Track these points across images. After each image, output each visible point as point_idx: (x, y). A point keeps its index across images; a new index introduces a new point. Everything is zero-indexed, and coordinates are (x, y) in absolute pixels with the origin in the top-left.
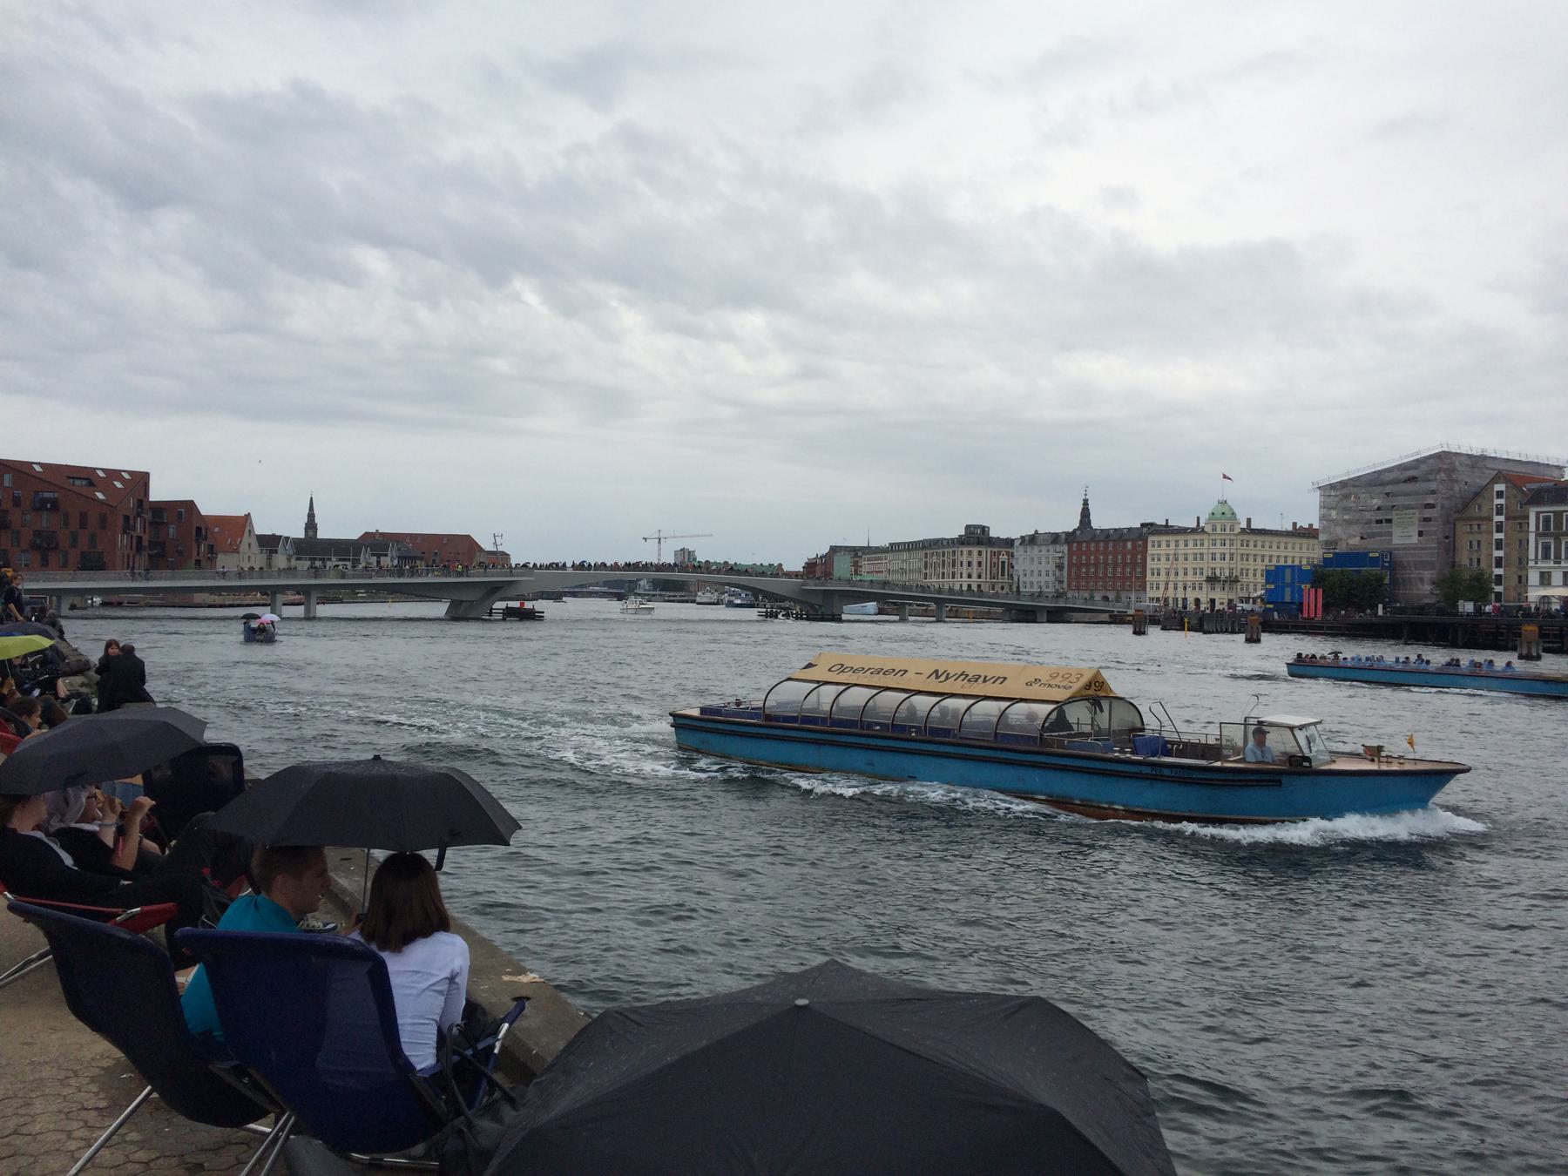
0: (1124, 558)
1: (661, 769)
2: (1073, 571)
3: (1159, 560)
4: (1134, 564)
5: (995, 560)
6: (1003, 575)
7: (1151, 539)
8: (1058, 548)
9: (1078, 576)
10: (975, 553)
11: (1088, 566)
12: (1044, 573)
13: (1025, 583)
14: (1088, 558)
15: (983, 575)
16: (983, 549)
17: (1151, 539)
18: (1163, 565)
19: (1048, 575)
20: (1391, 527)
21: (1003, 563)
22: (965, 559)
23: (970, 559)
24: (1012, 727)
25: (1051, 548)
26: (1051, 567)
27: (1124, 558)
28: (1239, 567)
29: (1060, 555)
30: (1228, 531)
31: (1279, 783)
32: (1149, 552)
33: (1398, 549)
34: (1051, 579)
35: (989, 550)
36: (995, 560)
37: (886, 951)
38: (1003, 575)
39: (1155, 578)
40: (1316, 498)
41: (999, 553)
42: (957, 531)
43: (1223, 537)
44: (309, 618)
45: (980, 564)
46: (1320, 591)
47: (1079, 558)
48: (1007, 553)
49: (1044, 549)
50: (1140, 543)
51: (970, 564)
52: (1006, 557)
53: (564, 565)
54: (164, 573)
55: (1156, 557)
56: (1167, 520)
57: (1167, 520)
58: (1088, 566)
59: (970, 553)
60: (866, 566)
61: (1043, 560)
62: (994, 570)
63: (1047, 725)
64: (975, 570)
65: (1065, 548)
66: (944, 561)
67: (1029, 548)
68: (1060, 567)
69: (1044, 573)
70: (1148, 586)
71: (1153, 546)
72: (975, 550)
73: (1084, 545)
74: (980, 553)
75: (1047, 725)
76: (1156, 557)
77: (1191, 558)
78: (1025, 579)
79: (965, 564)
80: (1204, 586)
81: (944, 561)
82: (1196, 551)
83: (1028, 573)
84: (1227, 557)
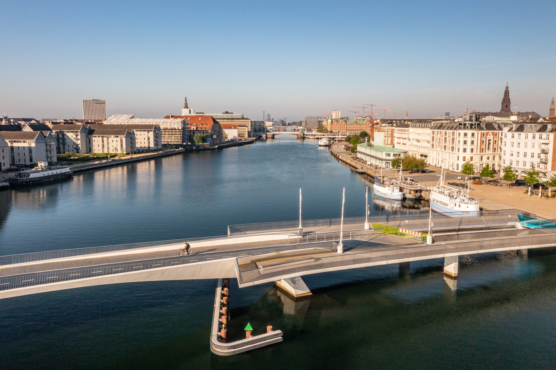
1: (345, 151)
16: (475, 132)
22: (462, 139)
24: (126, 165)
25: (537, 135)
31: (226, 112)
35: (480, 132)
37: (494, 202)
41: (487, 134)
42: (525, 112)
45: (472, 142)
48: (493, 134)
49: (530, 135)
51: (465, 142)
52: (492, 136)
59: (466, 135)
60: (97, 141)
63: (279, 293)
64: (469, 147)
66: (445, 138)
67: (516, 134)
72: (469, 132)
74: (473, 135)
75: (279, 293)
81: (445, 138)
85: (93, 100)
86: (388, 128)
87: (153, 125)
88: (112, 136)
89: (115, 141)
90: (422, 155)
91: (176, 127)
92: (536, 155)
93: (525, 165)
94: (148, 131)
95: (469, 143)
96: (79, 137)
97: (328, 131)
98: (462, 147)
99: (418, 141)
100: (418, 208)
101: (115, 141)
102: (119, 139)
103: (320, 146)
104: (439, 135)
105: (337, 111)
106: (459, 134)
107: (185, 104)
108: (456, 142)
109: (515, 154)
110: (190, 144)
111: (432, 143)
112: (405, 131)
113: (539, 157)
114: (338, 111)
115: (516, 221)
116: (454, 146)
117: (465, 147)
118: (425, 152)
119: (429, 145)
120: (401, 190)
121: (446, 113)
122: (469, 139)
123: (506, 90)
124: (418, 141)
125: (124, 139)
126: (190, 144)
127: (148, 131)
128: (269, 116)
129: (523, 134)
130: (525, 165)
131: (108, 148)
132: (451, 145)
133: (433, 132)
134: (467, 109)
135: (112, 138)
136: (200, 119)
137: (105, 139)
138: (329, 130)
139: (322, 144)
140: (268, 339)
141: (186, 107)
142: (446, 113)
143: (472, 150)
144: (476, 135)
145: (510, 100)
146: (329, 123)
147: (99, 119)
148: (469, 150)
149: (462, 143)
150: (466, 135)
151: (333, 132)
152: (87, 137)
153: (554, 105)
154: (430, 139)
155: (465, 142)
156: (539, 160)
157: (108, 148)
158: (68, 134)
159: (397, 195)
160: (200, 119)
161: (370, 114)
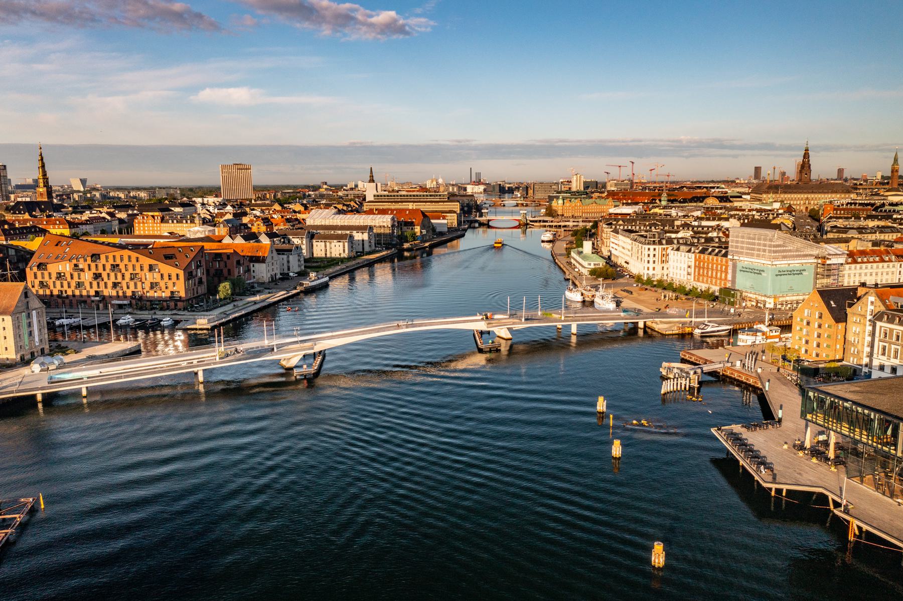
22: (647, 253)
35: (661, 247)
41: (667, 248)
45: (654, 255)
51: (649, 255)
59: (649, 249)
64: (651, 259)
67: (676, 252)
74: (655, 249)
85: (235, 164)
86: (607, 230)
87: (367, 226)
88: (335, 241)
89: (337, 246)
90: (626, 262)
91: (385, 224)
93: (680, 276)
94: (363, 233)
95: (652, 256)
96: (304, 242)
97: (558, 215)
98: (646, 259)
99: (623, 248)
101: (337, 246)
102: (341, 244)
103: (543, 241)
105: (578, 175)
107: (370, 176)
112: (616, 237)
115: (620, 312)
117: (649, 259)
118: (628, 259)
119: (629, 253)
120: (582, 294)
121: (756, 167)
122: (652, 253)
123: (805, 154)
124: (623, 248)
125: (346, 244)
127: (363, 233)
128: (478, 175)
130: (680, 276)
131: (331, 253)
134: (774, 169)
135: (335, 242)
136: (407, 212)
137: (328, 244)
138: (560, 213)
139: (546, 239)
141: (372, 180)
142: (756, 167)
143: (654, 262)
144: (657, 250)
145: (811, 167)
146: (560, 205)
148: (651, 262)
149: (646, 255)
150: (649, 249)
151: (565, 215)
152: (310, 242)
153: (898, 165)
154: (630, 249)
155: (649, 255)
157: (331, 253)
158: (293, 240)
159: (580, 298)
160: (407, 212)
161: (631, 177)
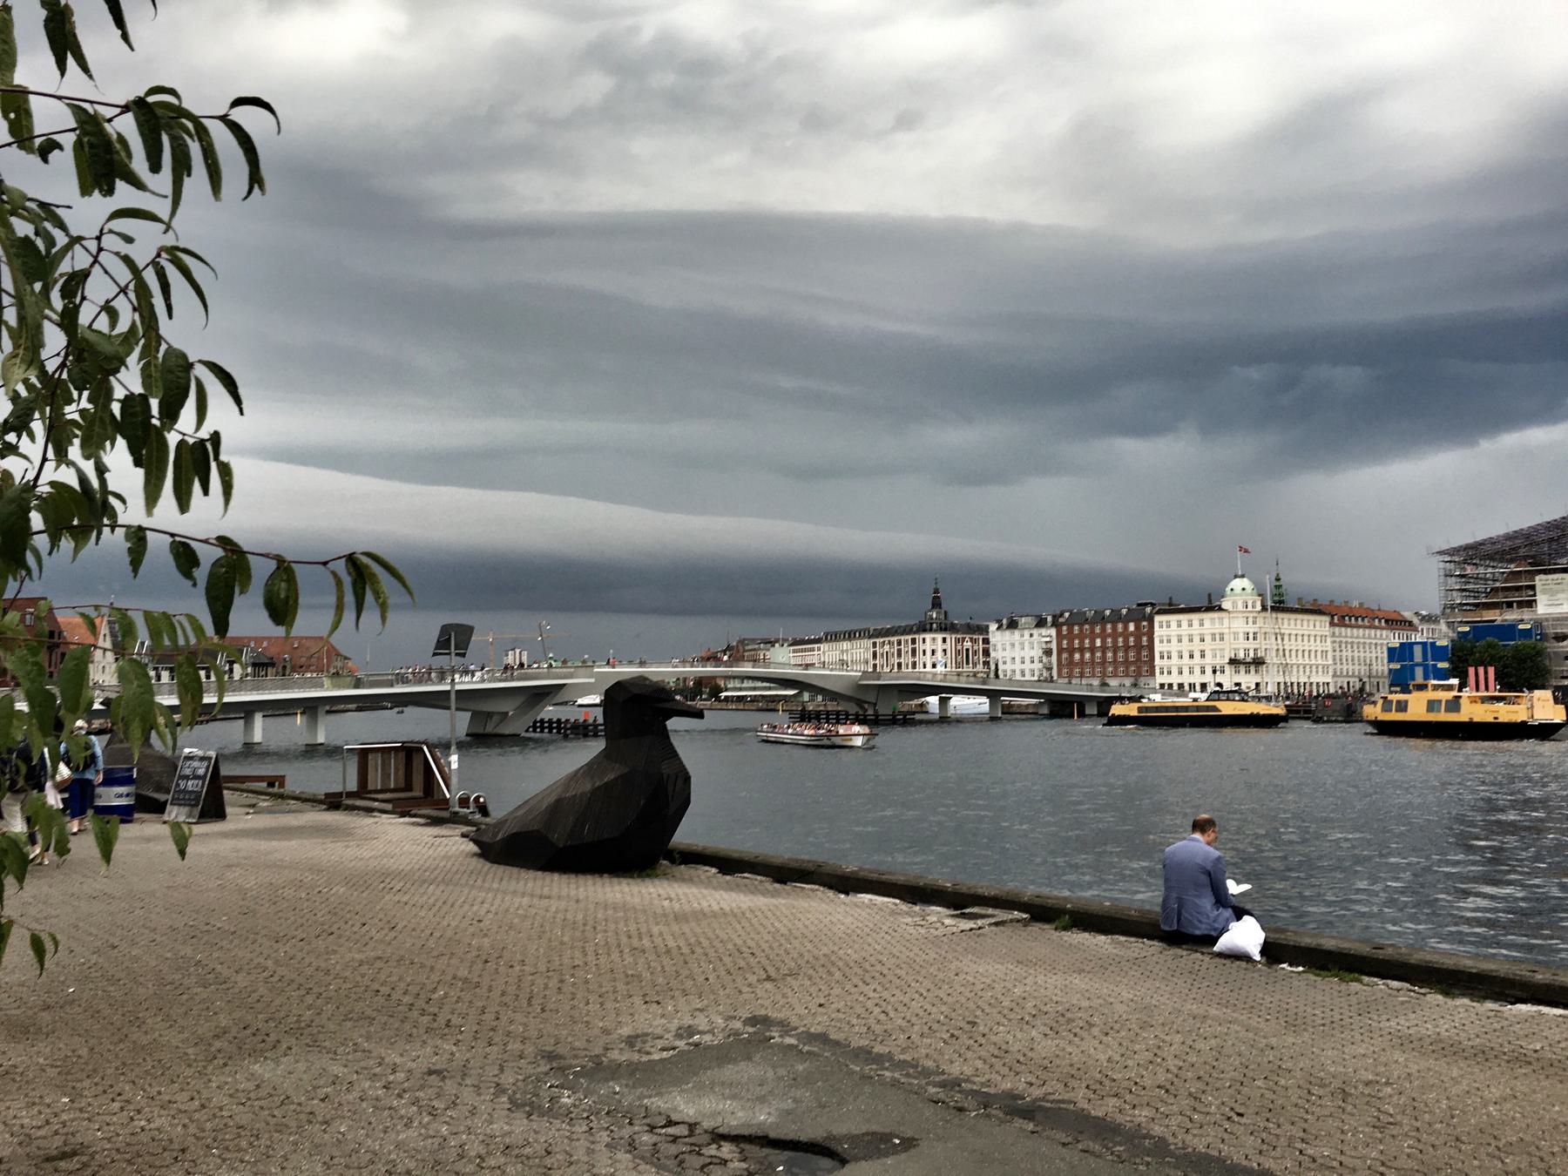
0: (1126, 641)
2: (1065, 655)
3: (1169, 641)
4: (1138, 647)
5: (959, 647)
6: (968, 663)
7: (1157, 619)
8: (1044, 631)
9: (1071, 663)
10: (940, 641)
11: (1082, 650)
12: (1027, 660)
13: (1005, 671)
14: (1082, 642)
15: (949, 665)
17: (1157, 619)
18: (1174, 647)
19: (1032, 662)
20: (1535, 595)
21: (967, 650)
23: (934, 647)
25: (1036, 632)
26: (1037, 653)
27: (1126, 641)
28: (1264, 647)
29: (1048, 639)
30: (1250, 608)
32: (1156, 634)
33: (1547, 620)
34: (1037, 666)
35: (954, 636)
36: (959, 647)
38: (968, 663)
39: (1165, 662)
40: (1436, 566)
41: (964, 639)
43: (1247, 615)
44: (403, 743)
46: (1491, 670)
47: (1071, 643)
49: (1027, 633)
50: (1145, 623)
52: (969, 643)
53: (1393, 654)
54: (246, 690)
55: (1165, 639)
56: (1171, 599)
57: (1171, 599)
58: (1082, 650)
61: (1027, 644)
62: (959, 658)
65: (1053, 632)
68: (1048, 652)
69: (1027, 660)
70: (1157, 671)
71: (1161, 627)
72: (939, 637)
73: (1076, 628)
74: (944, 640)
76: (1165, 639)
77: (1208, 638)
78: (1005, 667)
79: (929, 653)
80: (1227, 668)
82: (1247, 630)
83: (1009, 661)
84: (1251, 636)
92: (1036, 660)
100: (699, 714)
104: (887, 648)
105: (518, 651)
106: (924, 639)
108: (919, 653)
109: (1197, 655)
110: (1246, 887)
111: (872, 663)
113: (1041, 661)
114: (520, 653)
116: (917, 659)
122: (939, 646)
126: (1246, 887)
129: (1017, 633)
132: (911, 660)
133: (874, 644)
140: (440, 703)
144: (948, 640)
147: (1481, 670)
156: (1041, 665)
